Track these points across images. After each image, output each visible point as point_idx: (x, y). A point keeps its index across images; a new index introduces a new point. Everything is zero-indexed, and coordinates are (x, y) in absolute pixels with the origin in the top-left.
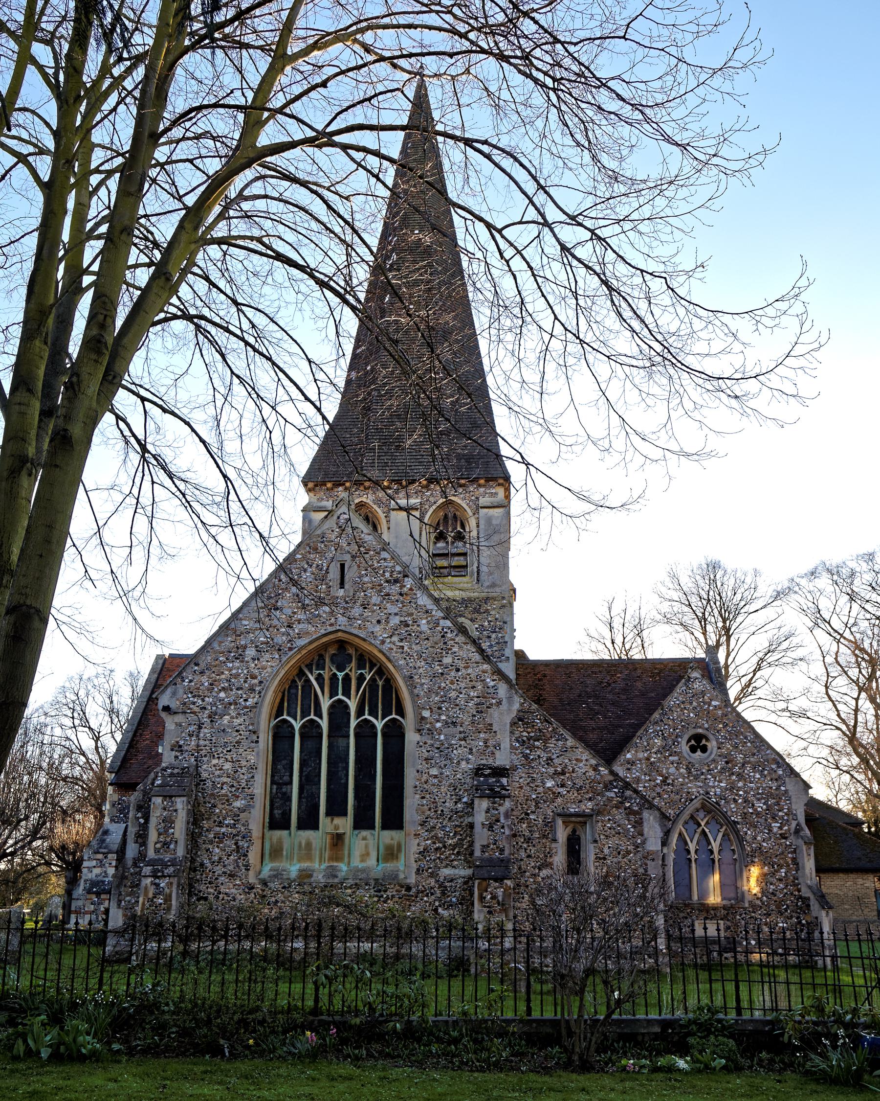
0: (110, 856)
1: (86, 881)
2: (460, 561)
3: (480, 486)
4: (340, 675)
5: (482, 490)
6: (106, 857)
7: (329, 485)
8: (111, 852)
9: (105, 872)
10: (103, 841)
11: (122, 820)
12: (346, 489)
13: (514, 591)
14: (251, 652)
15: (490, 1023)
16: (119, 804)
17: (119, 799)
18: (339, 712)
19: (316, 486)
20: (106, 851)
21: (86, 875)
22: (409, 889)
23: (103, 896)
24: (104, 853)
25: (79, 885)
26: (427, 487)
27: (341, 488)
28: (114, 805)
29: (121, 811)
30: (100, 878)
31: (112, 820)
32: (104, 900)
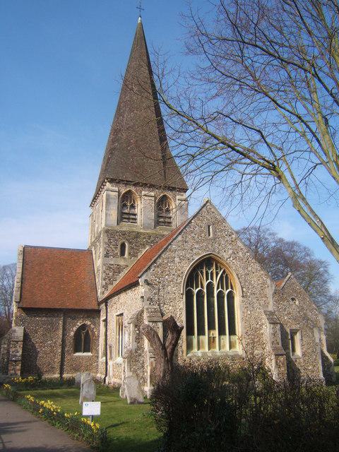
4: (210, 272)
14: (177, 260)
18: (210, 286)
22: (243, 359)
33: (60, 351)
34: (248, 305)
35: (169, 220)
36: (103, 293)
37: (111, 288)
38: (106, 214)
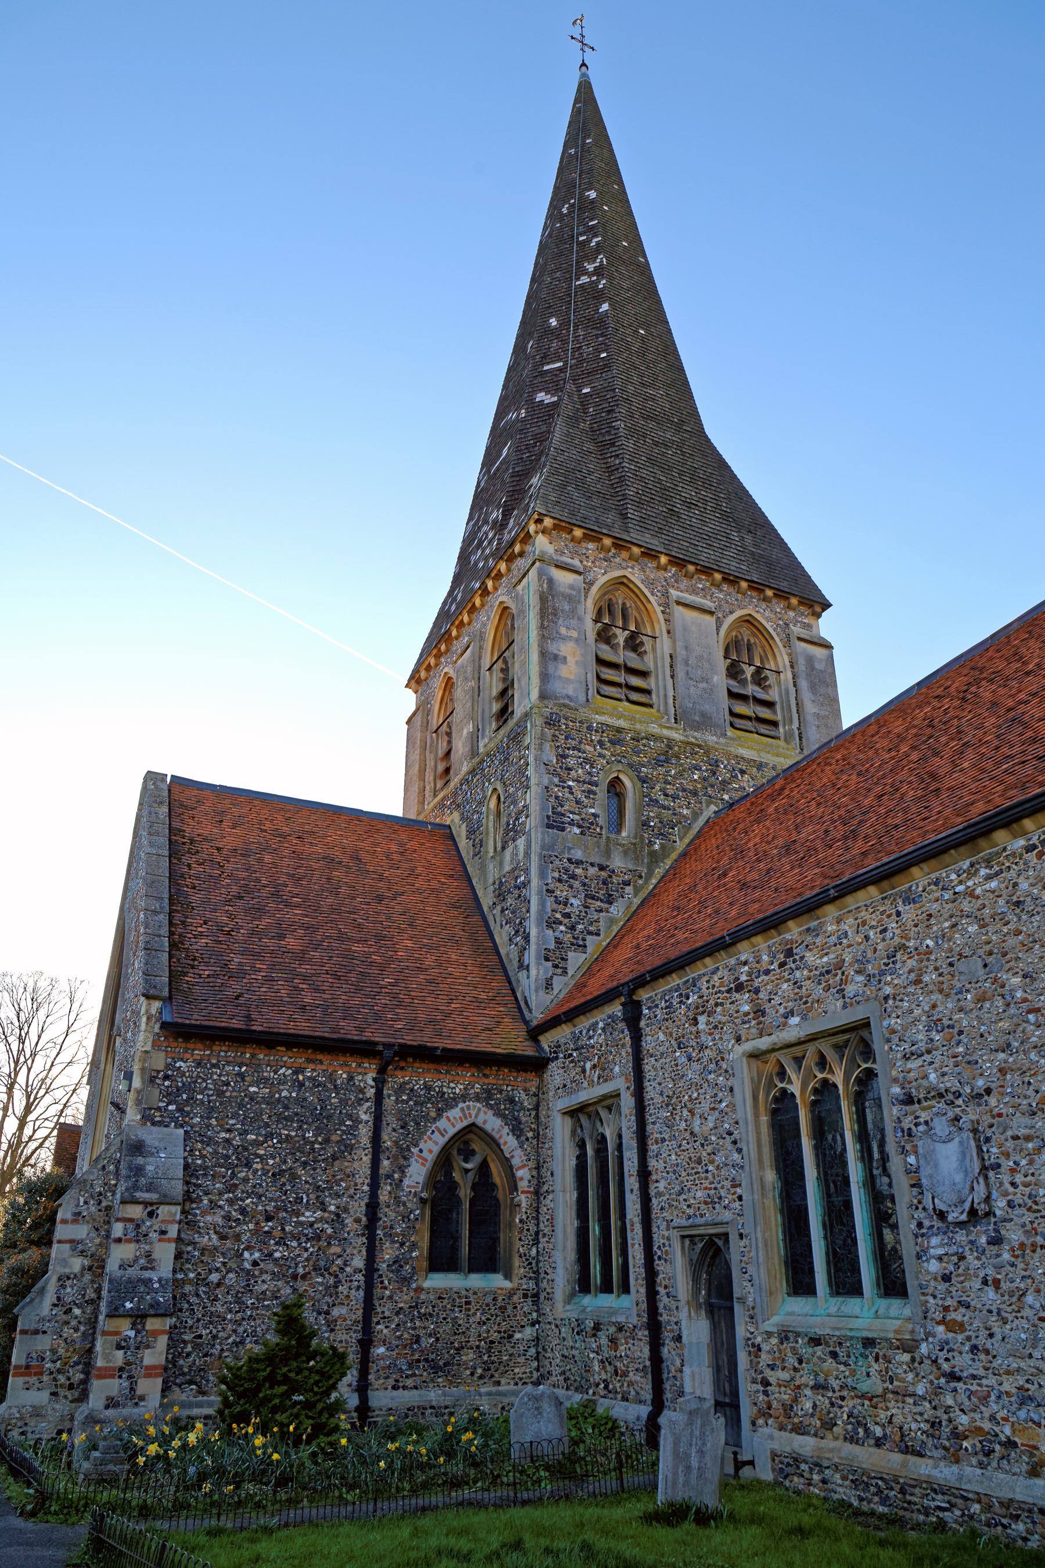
0: (163, 1211)
1: (63, 1279)
2: (765, 713)
3: (789, 607)
5: (792, 614)
6: (151, 1214)
7: (578, 533)
8: (166, 1200)
9: (148, 1255)
10: (139, 1171)
11: (175, 1120)
12: (602, 549)
13: (408, 722)
15: (545, 1444)
16: (166, 1077)
17: (168, 1066)
19: (556, 527)
20: (153, 1197)
21: (64, 1262)
23: (152, 1324)
24: (146, 1204)
25: (42, 1291)
26: (718, 586)
27: (591, 546)
28: (152, 1080)
29: (170, 1096)
30: (133, 1272)
31: (147, 1118)
32: (155, 1333)
33: (359, 1262)
34: (23, 1323)
35: (765, 713)
36: (548, 985)
37: (576, 960)
38: (543, 654)
